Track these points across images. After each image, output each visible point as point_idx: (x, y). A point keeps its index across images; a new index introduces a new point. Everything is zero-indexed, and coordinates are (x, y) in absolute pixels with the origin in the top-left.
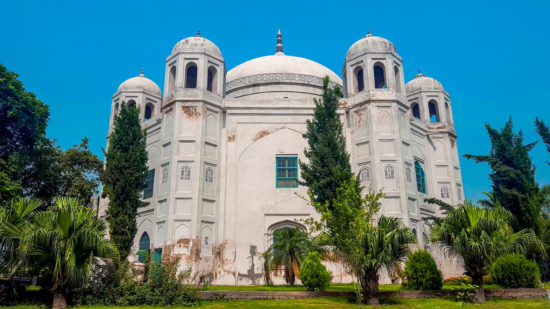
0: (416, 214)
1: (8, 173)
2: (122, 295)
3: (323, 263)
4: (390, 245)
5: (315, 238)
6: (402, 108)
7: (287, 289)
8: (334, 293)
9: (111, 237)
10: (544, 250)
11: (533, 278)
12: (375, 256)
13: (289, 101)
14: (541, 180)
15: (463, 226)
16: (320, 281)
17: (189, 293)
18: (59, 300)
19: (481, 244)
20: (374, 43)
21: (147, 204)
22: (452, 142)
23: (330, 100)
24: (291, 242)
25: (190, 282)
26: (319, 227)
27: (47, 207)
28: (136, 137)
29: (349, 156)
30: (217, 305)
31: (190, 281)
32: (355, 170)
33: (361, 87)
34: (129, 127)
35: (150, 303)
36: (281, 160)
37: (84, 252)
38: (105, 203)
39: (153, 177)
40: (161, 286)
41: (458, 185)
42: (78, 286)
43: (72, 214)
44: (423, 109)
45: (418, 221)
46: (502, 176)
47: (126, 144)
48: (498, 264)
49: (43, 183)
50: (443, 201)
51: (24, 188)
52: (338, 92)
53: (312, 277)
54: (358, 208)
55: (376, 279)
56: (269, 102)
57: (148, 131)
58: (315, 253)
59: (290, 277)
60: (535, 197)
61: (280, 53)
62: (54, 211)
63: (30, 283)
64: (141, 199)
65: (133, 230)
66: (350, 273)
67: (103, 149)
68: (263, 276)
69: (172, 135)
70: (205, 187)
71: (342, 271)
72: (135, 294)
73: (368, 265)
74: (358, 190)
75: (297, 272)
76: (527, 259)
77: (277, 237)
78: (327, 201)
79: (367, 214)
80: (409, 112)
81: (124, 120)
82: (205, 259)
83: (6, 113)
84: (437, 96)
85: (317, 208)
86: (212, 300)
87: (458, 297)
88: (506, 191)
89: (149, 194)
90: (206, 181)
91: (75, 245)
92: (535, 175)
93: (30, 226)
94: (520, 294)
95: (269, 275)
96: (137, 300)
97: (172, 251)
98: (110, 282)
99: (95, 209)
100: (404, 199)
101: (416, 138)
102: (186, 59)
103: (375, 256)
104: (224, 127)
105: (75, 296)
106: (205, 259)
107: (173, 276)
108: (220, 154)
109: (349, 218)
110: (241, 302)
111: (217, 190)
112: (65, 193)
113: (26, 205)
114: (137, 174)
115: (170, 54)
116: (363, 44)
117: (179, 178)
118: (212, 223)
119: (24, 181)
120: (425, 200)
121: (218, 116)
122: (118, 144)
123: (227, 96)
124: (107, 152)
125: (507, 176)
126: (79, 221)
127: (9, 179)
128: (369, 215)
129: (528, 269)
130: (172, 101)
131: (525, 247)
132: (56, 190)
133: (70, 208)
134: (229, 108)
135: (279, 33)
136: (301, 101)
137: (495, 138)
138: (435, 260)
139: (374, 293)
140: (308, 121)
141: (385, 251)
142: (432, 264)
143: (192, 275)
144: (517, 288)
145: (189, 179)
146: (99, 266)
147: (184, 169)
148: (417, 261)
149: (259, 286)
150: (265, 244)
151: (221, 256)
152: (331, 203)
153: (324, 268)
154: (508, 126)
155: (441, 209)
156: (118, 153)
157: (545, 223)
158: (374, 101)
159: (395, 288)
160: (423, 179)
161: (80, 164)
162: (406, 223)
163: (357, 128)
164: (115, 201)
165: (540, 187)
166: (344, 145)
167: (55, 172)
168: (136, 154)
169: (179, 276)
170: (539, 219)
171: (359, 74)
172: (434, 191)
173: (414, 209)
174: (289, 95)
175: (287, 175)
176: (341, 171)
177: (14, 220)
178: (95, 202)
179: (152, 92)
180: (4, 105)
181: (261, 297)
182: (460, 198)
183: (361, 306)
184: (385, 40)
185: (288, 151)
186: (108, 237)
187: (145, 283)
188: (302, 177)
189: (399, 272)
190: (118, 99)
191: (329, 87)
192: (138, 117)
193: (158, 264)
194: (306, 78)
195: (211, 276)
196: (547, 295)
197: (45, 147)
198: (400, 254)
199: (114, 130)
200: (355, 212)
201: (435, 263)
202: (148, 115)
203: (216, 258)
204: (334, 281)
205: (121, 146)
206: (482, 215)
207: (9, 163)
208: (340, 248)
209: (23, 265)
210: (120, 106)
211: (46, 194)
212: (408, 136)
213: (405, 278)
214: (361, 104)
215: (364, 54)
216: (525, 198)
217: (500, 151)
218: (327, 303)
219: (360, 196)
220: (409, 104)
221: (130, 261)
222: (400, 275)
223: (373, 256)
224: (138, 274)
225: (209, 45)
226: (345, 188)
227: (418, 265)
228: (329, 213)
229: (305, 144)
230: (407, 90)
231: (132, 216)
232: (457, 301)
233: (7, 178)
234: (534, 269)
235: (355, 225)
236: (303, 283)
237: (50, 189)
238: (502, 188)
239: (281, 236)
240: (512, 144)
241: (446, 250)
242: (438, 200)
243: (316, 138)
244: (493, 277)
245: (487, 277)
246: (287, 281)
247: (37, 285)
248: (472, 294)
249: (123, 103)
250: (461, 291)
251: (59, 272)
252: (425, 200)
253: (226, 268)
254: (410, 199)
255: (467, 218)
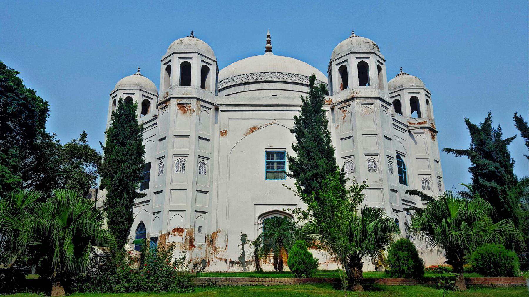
0: (399, 205)
1: (8, 166)
2: (118, 282)
3: (310, 251)
4: (373, 234)
5: (302, 227)
6: (384, 104)
7: (275, 275)
8: (320, 279)
9: (109, 227)
10: (523, 240)
11: (513, 267)
12: (360, 244)
13: (277, 98)
14: (520, 172)
15: (444, 216)
16: (307, 268)
17: (183, 280)
18: (57, 287)
19: (461, 234)
20: (358, 43)
21: (144, 195)
22: (433, 137)
23: (316, 97)
24: (280, 230)
25: (184, 269)
26: (305, 216)
27: (46, 198)
28: (133, 132)
29: (334, 150)
30: (209, 291)
31: (184, 268)
32: (339, 162)
33: (345, 85)
34: (126, 122)
35: (145, 290)
36: (269, 154)
37: (82, 242)
38: (103, 194)
39: (150, 170)
40: (156, 273)
41: (439, 177)
42: (76, 274)
43: (71, 205)
44: (405, 105)
45: (400, 211)
46: (481, 169)
47: (123, 139)
48: (478, 253)
49: (42, 176)
50: (423, 192)
51: (24, 180)
52: (324, 90)
53: (299, 264)
54: (343, 199)
55: (360, 266)
56: (259, 99)
57: (145, 126)
58: (302, 241)
59: (278, 263)
60: (514, 189)
61: (269, 53)
62: (53, 203)
63: (30, 272)
64: (138, 191)
65: (131, 220)
66: (336, 260)
67: (101, 143)
68: (253, 263)
69: (168, 130)
70: (199, 179)
71: (328, 259)
72: (131, 282)
73: (352, 253)
74: (343, 182)
75: (285, 259)
76: (506, 249)
77: (267, 226)
78: (313, 192)
79: (351, 204)
80: (392, 108)
81: (122, 115)
82: (199, 247)
83: (7, 109)
84: (419, 93)
85: (304, 199)
86: (204, 287)
87: (439, 285)
88: (486, 183)
89: (146, 186)
90: (200, 173)
91: (73, 235)
92: (513, 168)
93: (30, 217)
94: (500, 282)
95: (259, 262)
96: (133, 287)
97: (167, 240)
98: (107, 270)
99: (93, 200)
100: (386, 190)
101: (399, 133)
102: (180, 58)
103: (358, 245)
104: (217, 123)
105: (73, 284)
106: (199, 247)
107: (168, 262)
108: (213, 147)
109: (334, 209)
110: (232, 288)
111: (210, 181)
112: (64, 186)
113: (26, 197)
114: (134, 167)
115: (166, 53)
116: (347, 44)
117: (175, 170)
118: (206, 213)
119: (24, 174)
120: (407, 192)
121: (212, 112)
122: (116, 139)
123: (219, 94)
124: (105, 146)
125: (487, 168)
126: (78, 212)
127: (10, 172)
128: (353, 206)
129: (507, 258)
130: (168, 98)
131: (504, 237)
132: (56, 182)
133: (68, 200)
134: (221, 105)
135: (268, 34)
136: (289, 98)
137: (474, 133)
138: (417, 249)
139: (358, 279)
140: (295, 118)
141: (369, 240)
142: (414, 252)
143: (186, 262)
144: (497, 276)
145: (183, 171)
146: (96, 255)
147: (179, 163)
148: (399, 250)
149: (249, 273)
150: (255, 232)
151: (214, 244)
152: (317, 194)
153: (311, 255)
154: (488, 121)
155: (422, 200)
156: (116, 147)
157: (523, 214)
158: (357, 98)
159: (378, 275)
160: (405, 172)
161: (78, 157)
162: (388, 213)
163: (341, 123)
164: (113, 192)
165: (519, 179)
166: (329, 139)
167: (55, 166)
168: (133, 148)
169: (174, 263)
170: (518, 211)
171: (344, 71)
172: (414, 183)
173: (396, 200)
174: (277, 93)
175: (275, 168)
176: (326, 164)
177: (15, 212)
178: (93, 193)
179: (149, 90)
180: (5, 101)
181: (252, 283)
182: (440, 189)
183: (346, 292)
184: (369, 40)
185: (276, 145)
186: (105, 227)
187: (141, 271)
188: (290, 170)
189: (382, 259)
190: (116, 96)
191: (315, 86)
192: (135, 113)
193: (154, 251)
194: (294, 76)
195: (205, 263)
196: (526, 284)
197: (44, 141)
198: (383, 242)
199: (111, 126)
200: (339, 202)
201: (417, 252)
202: (145, 111)
203: (209, 245)
204: (321, 267)
205: (119, 140)
206: (462, 206)
207: (10, 157)
208: (326, 236)
209: (23, 254)
210: (117, 103)
211: (46, 186)
212: (391, 132)
213: (388, 266)
214: (345, 101)
215: (348, 54)
216: (504, 190)
217: (480, 145)
218: (314, 289)
219: (344, 187)
220: (391, 101)
221: (126, 249)
222: (383, 263)
223: (357, 244)
224: (134, 262)
225: (202, 46)
226: (330, 180)
227: (401, 254)
228: (315, 203)
229: (293, 139)
230: (389, 87)
231: (130, 205)
232: (438, 288)
233: (7, 171)
234: (513, 259)
235: (339, 215)
236: (291, 270)
237: (49, 182)
238: (482, 181)
239: (270, 225)
240: (491, 138)
241: (427, 239)
242: (419, 192)
243: (303, 133)
244: (473, 266)
245: (467, 266)
246: (276, 268)
247: (36, 273)
248: (453, 282)
249: (121, 99)
250: (443, 278)
251: (58, 261)
252: (407, 192)
253: (218, 255)
254: (392, 190)
255: (448, 209)
